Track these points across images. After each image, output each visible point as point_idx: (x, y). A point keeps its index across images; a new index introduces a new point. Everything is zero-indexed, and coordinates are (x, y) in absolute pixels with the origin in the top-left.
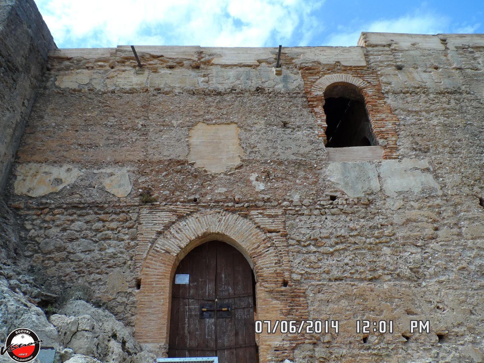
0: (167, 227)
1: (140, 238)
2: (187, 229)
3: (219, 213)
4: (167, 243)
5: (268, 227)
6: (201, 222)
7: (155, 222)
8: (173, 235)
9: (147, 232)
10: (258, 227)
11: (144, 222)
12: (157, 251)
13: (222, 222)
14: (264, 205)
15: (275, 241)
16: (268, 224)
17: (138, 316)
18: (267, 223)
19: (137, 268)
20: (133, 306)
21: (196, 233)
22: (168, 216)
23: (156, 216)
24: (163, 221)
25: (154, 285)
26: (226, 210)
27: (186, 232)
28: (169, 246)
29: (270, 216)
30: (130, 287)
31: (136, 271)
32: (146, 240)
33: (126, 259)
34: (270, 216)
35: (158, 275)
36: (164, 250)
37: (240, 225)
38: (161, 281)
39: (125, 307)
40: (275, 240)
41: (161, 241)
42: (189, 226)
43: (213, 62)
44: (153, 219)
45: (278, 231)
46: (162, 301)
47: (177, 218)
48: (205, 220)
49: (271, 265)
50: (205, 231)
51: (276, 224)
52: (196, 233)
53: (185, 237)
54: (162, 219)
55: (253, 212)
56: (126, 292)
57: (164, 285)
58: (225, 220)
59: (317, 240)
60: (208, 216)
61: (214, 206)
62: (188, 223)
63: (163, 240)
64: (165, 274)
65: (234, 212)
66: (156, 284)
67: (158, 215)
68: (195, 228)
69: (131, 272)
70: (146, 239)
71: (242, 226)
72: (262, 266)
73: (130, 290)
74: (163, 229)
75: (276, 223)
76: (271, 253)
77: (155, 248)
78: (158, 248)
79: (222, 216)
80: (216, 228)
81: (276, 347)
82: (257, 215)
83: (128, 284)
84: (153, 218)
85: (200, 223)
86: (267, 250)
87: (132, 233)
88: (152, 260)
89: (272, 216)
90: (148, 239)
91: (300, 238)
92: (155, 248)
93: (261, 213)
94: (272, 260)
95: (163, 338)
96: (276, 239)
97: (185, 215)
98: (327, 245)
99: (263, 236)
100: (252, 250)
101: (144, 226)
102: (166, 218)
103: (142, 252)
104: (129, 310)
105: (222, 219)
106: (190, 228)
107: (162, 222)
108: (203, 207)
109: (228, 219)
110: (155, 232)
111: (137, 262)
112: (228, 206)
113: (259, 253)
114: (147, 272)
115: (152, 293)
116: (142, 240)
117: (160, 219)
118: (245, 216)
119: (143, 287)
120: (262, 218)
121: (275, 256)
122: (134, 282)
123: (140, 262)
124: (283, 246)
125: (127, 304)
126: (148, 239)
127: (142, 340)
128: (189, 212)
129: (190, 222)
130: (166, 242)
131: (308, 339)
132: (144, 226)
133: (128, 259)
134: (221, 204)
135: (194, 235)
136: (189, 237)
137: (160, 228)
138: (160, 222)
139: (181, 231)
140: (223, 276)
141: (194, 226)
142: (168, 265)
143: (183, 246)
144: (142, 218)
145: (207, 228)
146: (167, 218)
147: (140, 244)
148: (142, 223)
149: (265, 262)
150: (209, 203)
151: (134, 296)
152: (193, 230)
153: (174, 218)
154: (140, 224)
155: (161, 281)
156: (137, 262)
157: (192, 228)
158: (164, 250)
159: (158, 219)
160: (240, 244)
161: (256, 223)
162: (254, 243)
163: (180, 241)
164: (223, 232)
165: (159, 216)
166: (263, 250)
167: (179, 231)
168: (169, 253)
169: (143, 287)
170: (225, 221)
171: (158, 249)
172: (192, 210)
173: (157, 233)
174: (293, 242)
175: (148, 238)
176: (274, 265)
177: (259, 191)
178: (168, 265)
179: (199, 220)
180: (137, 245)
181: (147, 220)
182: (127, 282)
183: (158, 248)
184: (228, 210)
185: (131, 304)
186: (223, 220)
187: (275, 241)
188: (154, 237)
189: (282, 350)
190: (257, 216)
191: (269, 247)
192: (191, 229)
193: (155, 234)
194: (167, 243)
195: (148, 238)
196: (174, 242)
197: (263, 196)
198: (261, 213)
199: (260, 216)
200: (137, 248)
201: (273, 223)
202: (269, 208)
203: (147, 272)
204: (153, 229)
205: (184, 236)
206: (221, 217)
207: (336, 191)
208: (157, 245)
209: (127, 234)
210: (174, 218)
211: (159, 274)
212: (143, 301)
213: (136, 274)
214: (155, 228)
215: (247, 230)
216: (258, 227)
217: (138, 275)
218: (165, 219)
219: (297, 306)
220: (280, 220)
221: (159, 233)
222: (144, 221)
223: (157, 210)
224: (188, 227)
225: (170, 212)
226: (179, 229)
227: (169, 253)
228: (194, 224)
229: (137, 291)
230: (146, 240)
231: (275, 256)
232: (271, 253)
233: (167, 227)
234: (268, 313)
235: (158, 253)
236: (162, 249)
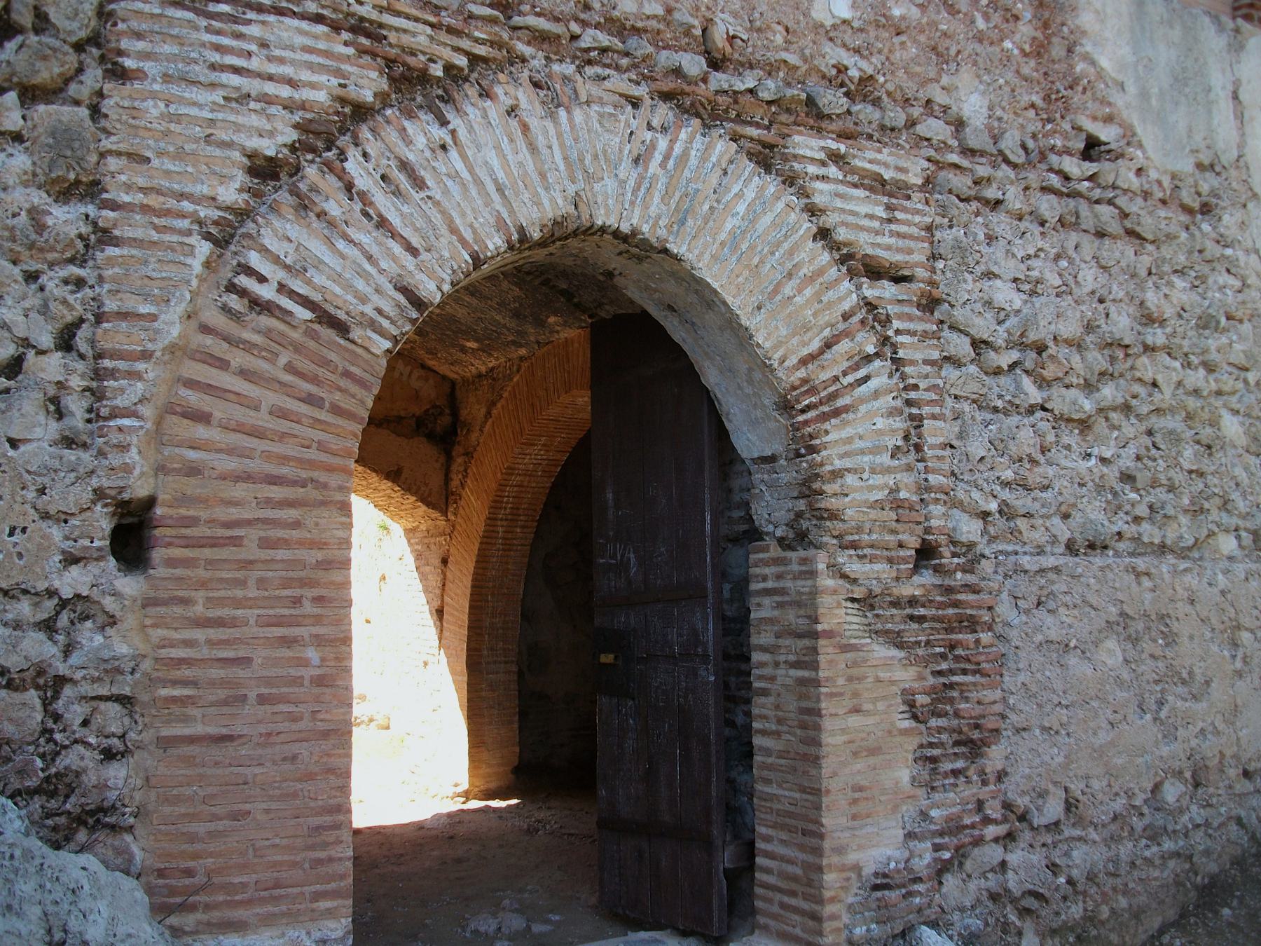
0: (329, 132)
1: (128, 187)
2: (455, 176)
3: (635, 103)
4: (328, 258)
5: (869, 244)
6: (541, 141)
7: (235, 80)
8: (364, 197)
9: (180, 155)
10: (823, 234)
11: (148, 66)
12: (256, 304)
13: (654, 166)
14: (849, 112)
15: (898, 332)
16: (869, 230)
17: (145, 759)
18: (857, 218)
19: (113, 416)
20: (104, 691)
21: (512, 212)
22: (327, 54)
23: (239, 36)
24: (292, 83)
25: (251, 551)
26: (666, 96)
27: (446, 191)
28: (338, 278)
29: (877, 185)
30: (71, 560)
31: (115, 438)
32: (167, 213)
33: (26, 343)
34: (877, 185)
35: (273, 480)
36: (306, 302)
37: (741, 208)
38: (297, 524)
39: (46, 704)
40: (896, 324)
41: (281, 235)
42: (464, 157)
43: (117, 232)
44: (216, 57)
45: (906, 273)
46: (312, 654)
47: (384, 85)
48: (559, 135)
49: (878, 460)
50: (565, 208)
51: (899, 235)
52: (512, 212)
53: (444, 231)
54: (287, 70)
55: (807, 145)
56: (51, 593)
57: (320, 555)
58: (667, 157)
59: (1041, 349)
60: (578, 115)
61: (604, 50)
62: (462, 133)
63: (293, 230)
64: (322, 476)
65: (709, 114)
66: (266, 544)
67: (254, 30)
68: (501, 175)
69: (69, 442)
70: (171, 203)
71: (752, 216)
72: (838, 464)
73: (72, 581)
74: (293, 148)
75: (903, 229)
76: (876, 395)
77: (244, 281)
78: (262, 279)
79: (650, 127)
80: (614, 206)
81: (885, 876)
82: (823, 164)
83: (56, 533)
84: (218, 48)
85: (533, 148)
86: (862, 373)
87: (64, 138)
88: (223, 364)
89: (883, 182)
90: (187, 206)
91: (983, 326)
92: (244, 281)
93: (836, 157)
94: (880, 433)
95: (335, 894)
96: (900, 317)
97: (437, 71)
98: (1075, 381)
99: (846, 294)
100: (796, 368)
101: (154, 96)
102: (310, 66)
103: (146, 297)
104: (85, 723)
105: (653, 146)
106: (471, 171)
107: (285, 92)
108: (540, 38)
109: (685, 155)
110: (236, 155)
111: (113, 374)
112: (677, 72)
113: (826, 384)
114: (192, 455)
115: (238, 603)
116: (145, 209)
117: (273, 69)
118: (765, 157)
119: (171, 563)
120: (842, 189)
121: (892, 412)
122: (102, 522)
123: (137, 376)
124: (926, 362)
125: (61, 681)
126: (187, 206)
127: (199, 916)
128: (462, 61)
129: (471, 130)
130: (317, 247)
131: (995, 822)
132: (154, 96)
133: (46, 339)
134: (642, 47)
135: (500, 225)
136: (468, 235)
137: (275, 137)
138: (270, 88)
139: (419, 184)
140: (610, 496)
141: (495, 163)
142: (336, 410)
143: (431, 290)
144: (139, 36)
145: (571, 190)
146: (322, 69)
147: (129, 232)
148: (139, 75)
149: (849, 440)
150: (575, 28)
151: (112, 621)
152: (491, 188)
153: (368, 83)
154: (119, 74)
155: (297, 524)
156: (113, 374)
157: (482, 174)
158: (306, 302)
159: (254, 64)
160: (745, 321)
161: (813, 211)
162: (806, 328)
163: (414, 252)
164: (662, 233)
165: (264, 45)
166: (845, 374)
167: (401, 179)
168: (342, 328)
169: (171, 563)
170: (671, 163)
171: (266, 292)
172: (482, 50)
173: (252, 171)
174: (960, 346)
175: (182, 196)
176: (885, 459)
177: (828, 23)
178: (336, 410)
179: (525, 128)
180: (105, 236)
181: (172, 58)
182: (46, 516)
183: (262, 279)
184: (678, 97)
185: (94, 680)
186: (658, 157)
187: (898, 332)
188: (230, 194)
189: (904, 886)
190: (821, 171)
191: (868, 359)
192: (478, 182)
193: (241, 178)
194: (328, 258)
195: (182, 196)
196: (374, 250)
197: (848, 59)
198: (836, 157)
199: (833, 171)
200: (110, 261)
201: (888, 228)
202: (870, 137)
203: (192, 455)
204: (222, 135)
205: (437, 219)
206: (649, 135)
207: (1109, 119)
208: (255, 259)
209: (18, 138)
210: (368, 83)
211: (284, 471)
212: (181, 662)
213: (115, 460)
214: (238, 128)
215: (779, 244)
216: (823, 234)
217: (127, 469)
218: (305, 75)
219: (965, 672)
220: (917, 219)
221: (265, 170)
222: (147, 56)
223: (226, 41)
224: (459, 165)
225: (336, 28)
226: (404, 166)
227: (342, 328)
228: (498, 148)
229: (130, 585)
230: (167, 213)
231: (892, 412)
232: (876, 395)
233: (329, 132)
234: (856, 710)
235: (265, 321)
236: (292, 294)
